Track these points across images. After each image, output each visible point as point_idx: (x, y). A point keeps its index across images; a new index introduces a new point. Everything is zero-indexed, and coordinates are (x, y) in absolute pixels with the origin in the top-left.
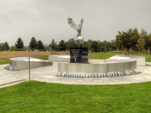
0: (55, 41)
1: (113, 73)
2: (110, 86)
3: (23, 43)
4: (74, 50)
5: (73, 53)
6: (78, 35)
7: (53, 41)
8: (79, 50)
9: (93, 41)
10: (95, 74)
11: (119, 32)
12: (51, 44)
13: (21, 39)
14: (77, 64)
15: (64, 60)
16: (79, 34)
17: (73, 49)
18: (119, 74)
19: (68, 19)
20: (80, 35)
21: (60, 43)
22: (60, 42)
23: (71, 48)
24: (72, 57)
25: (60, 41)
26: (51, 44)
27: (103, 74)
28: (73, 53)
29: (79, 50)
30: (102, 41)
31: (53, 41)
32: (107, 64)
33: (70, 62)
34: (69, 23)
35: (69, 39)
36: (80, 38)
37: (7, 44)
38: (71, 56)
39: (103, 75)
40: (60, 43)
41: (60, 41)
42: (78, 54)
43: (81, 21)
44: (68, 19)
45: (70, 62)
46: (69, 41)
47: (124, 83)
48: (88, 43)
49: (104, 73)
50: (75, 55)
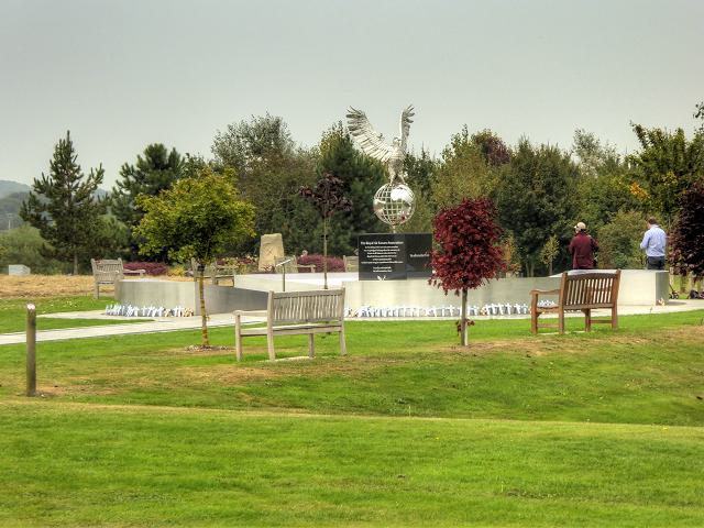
0: (85, 163)
1: (500, 306)
2: (530, 411)
5: (371, 260)
7: (64, 158)
9: (524, 148)
11: (639, 129)
12: (44, 199)
17: (370, 241)
18: (518, 309)
19: (348, 116)
21: (128, 185)
22: (127, 171)
25: (133, 163)
26: (44, 199)
28: (371, 260)
31: (64, 158)
35: (225, 131)
40: (128, 185)
41: (133, 163)
43: (403, 120)
44: (348, 116)
46: (224, 154)
48: (446, 172)
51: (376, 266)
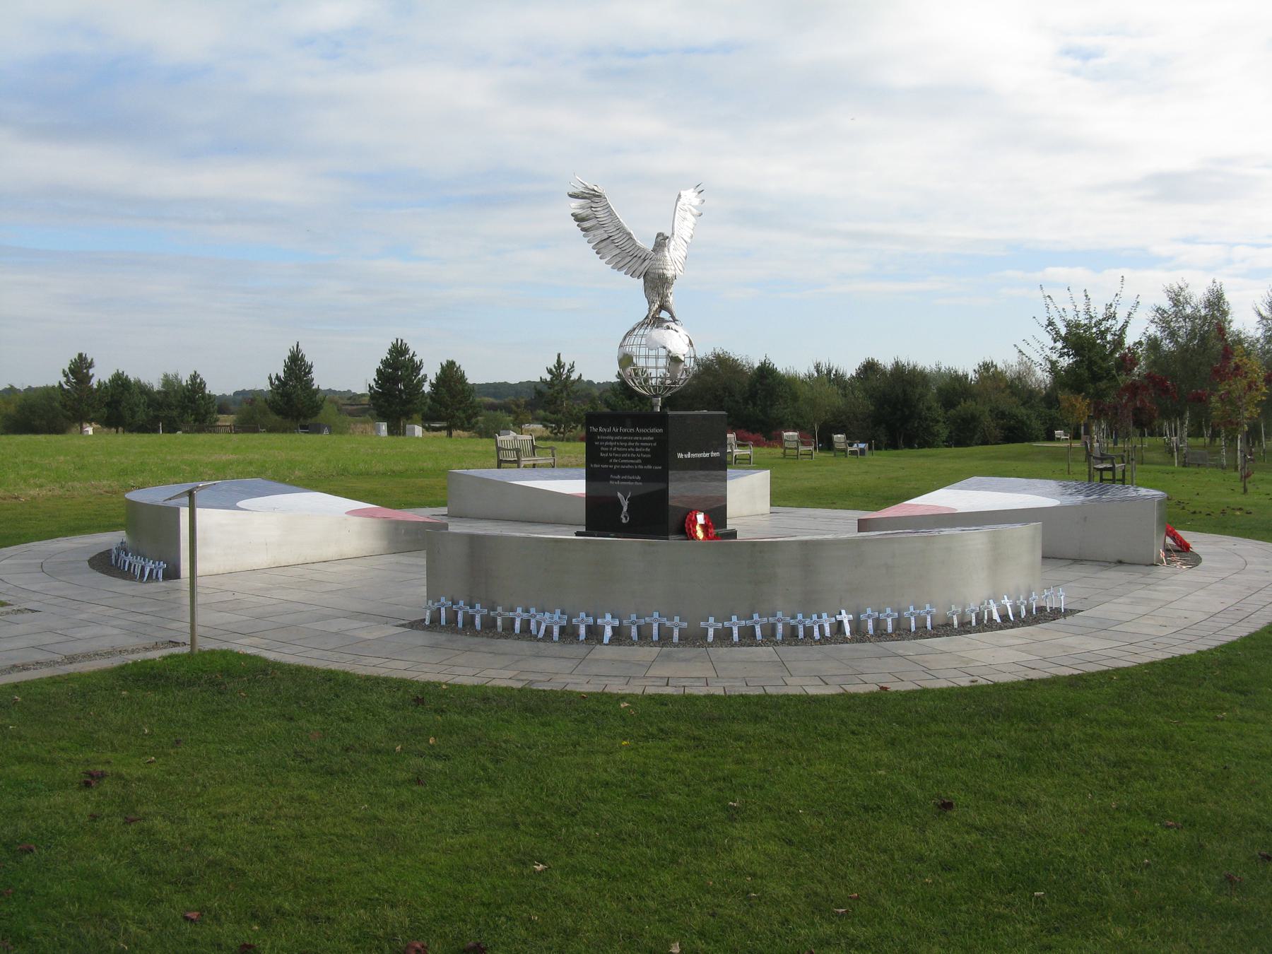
3: (463, 376)
4: (612, 434)
5: (606, 461)
6: (654, 321)
8: (652, 431)
9: (167, 381)
10: (727, 624)
13: (302, 359)
14: (649, 544)
15: (545, 509)
16: (663, 307)
20: (664, 315)
23: (592, 419)
24: (602, 489)
27: (472, 607)
28: (606, 461)
29: (652, 431)
30: (967, 365)
32: (473, 539)
33: (583, 529)
34: (586, 225)
36: (677, 341)
37: (765, 377)
38: (590, 478)
39: (469, 621)
42: (645, 461)
45: (583, 529)
47: (283, 660)
49: (478, 606)
50: (622, 472)
51: (616, 472)
